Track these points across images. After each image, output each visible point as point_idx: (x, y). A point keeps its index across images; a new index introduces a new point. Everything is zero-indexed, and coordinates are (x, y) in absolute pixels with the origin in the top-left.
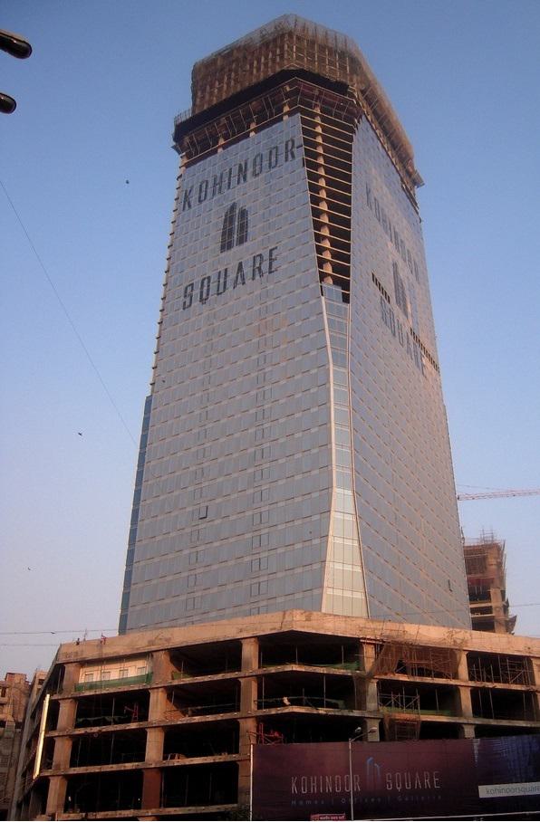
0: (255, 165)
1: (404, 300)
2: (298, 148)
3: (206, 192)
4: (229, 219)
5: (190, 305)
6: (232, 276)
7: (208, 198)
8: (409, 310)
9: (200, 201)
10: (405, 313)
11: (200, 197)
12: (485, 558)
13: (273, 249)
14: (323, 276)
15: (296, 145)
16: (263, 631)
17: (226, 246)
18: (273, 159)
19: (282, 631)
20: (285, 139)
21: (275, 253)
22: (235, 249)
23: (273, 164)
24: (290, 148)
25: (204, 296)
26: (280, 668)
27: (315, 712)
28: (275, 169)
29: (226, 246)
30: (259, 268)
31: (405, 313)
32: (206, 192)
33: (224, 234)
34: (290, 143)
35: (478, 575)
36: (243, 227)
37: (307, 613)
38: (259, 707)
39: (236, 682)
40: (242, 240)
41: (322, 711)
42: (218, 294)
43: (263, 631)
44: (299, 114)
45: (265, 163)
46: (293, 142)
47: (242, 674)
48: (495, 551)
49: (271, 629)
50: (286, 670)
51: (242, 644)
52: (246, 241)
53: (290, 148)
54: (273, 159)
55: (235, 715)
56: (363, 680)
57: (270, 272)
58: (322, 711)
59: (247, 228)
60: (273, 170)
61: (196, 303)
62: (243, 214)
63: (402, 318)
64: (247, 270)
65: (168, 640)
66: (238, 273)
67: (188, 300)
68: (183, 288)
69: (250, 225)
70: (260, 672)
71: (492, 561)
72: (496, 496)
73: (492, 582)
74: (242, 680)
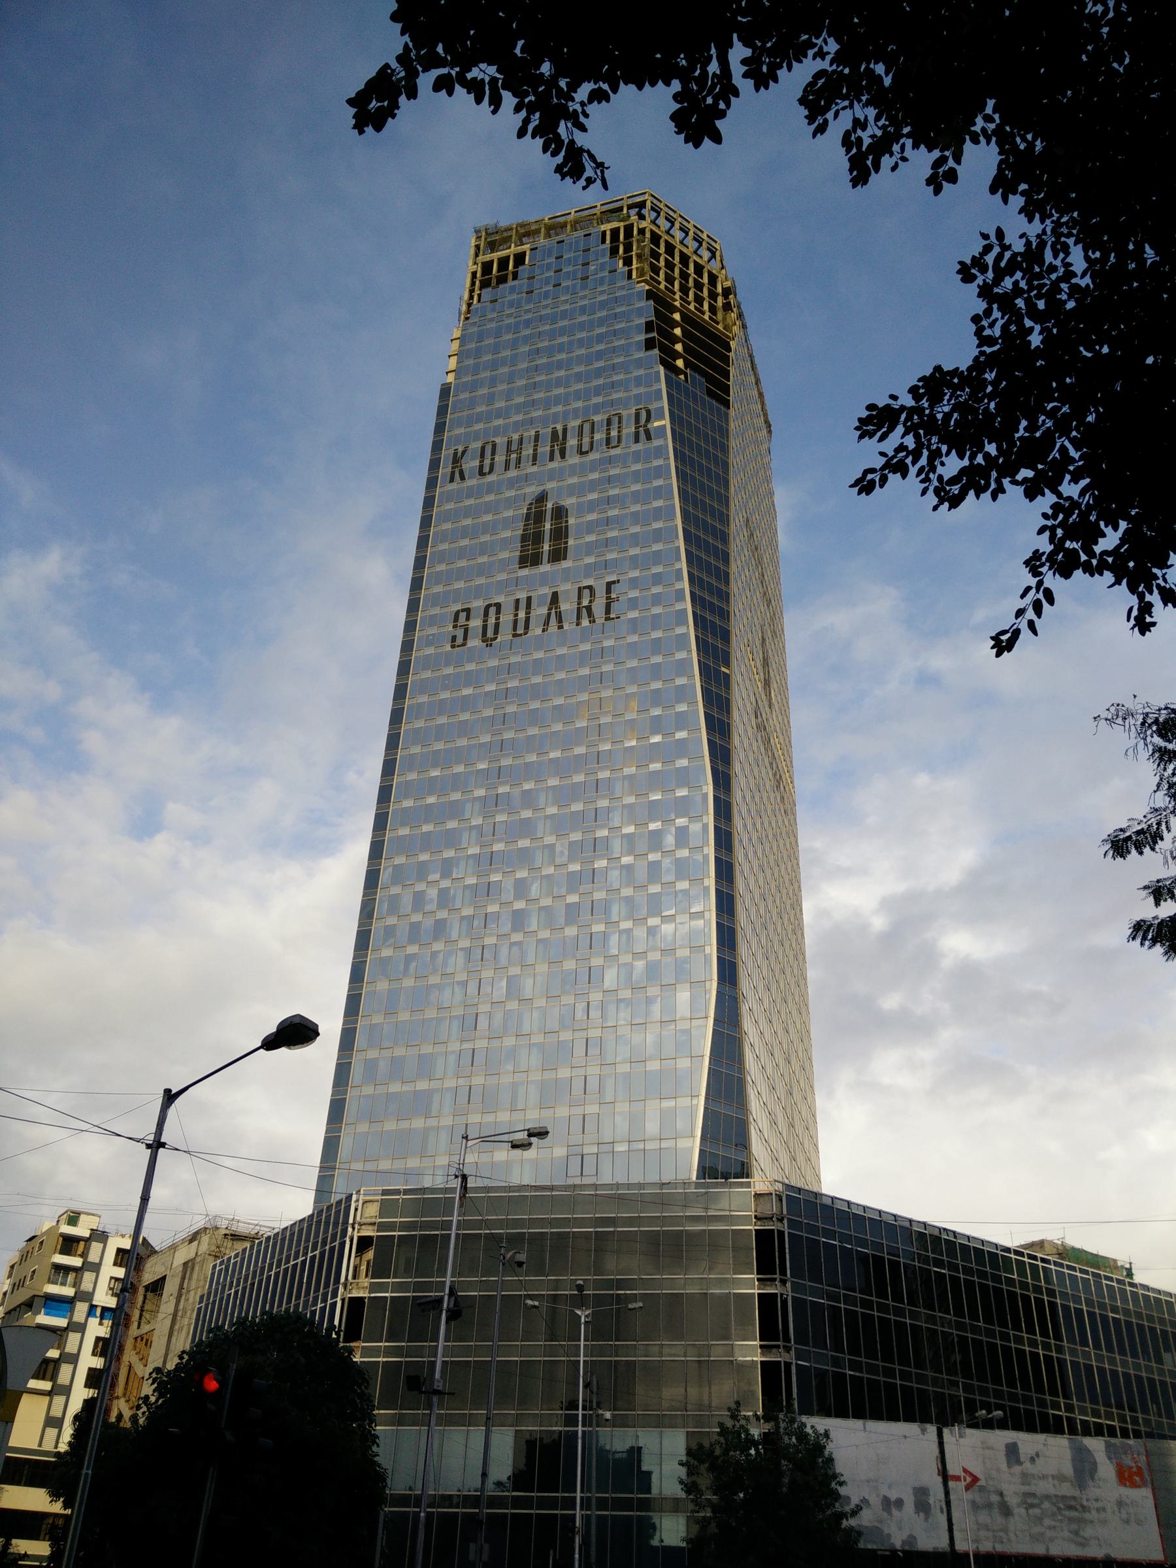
4: (535, 515)
17: (530, 559)
33: (524, 538)
36: (560, 534)
62: (560, 513)
66: (550, 609)
67: (460, 633)
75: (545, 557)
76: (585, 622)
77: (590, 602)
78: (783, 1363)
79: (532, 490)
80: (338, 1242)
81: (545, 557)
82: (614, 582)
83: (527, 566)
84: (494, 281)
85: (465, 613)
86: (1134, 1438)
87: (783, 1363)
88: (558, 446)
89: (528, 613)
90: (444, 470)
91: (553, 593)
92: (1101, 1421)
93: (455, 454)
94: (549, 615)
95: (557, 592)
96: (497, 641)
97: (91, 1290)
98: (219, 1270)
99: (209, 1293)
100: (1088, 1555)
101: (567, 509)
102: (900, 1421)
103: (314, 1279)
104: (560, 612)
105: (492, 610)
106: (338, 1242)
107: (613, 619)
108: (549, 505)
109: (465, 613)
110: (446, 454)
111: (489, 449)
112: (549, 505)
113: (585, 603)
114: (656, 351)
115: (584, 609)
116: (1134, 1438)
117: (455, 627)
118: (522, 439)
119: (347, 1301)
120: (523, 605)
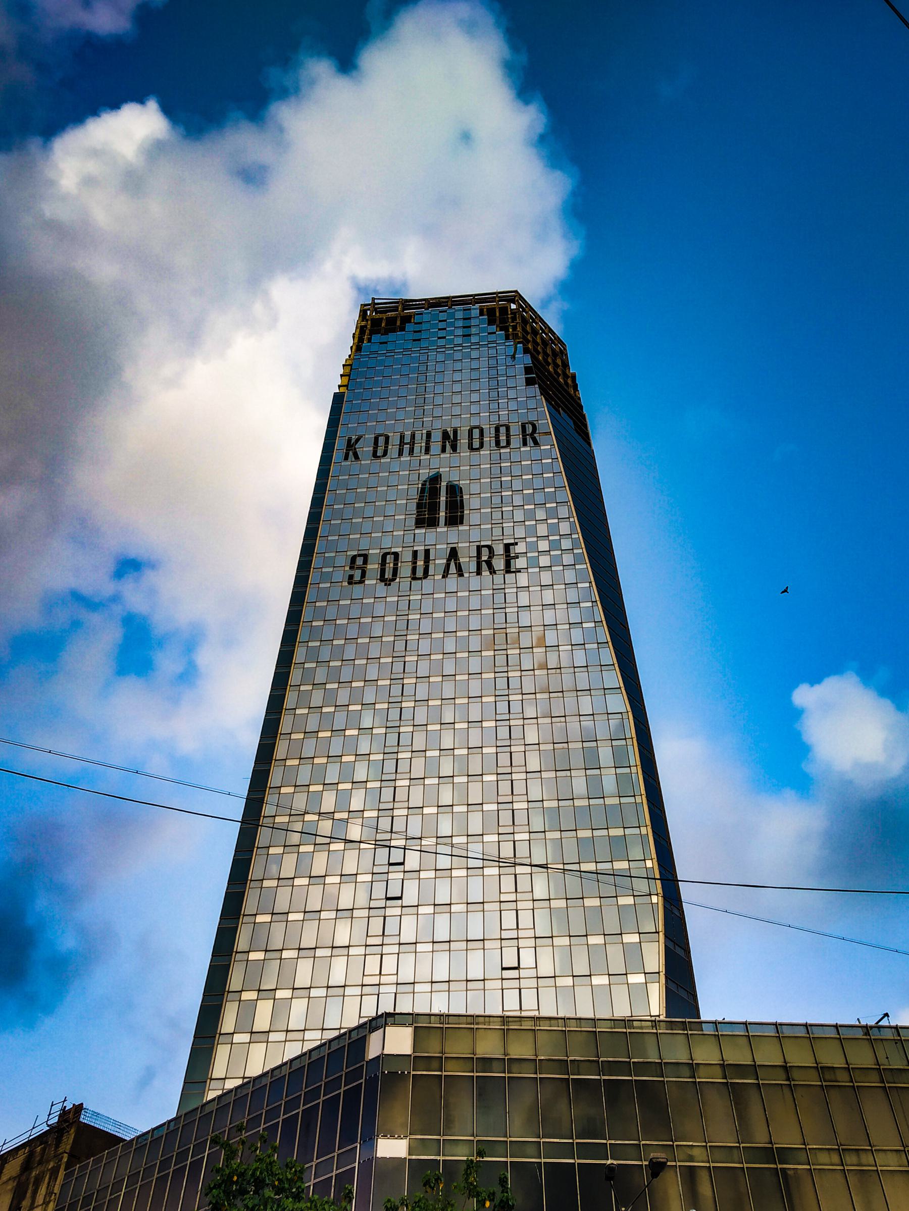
66: (449, 560)
75: (442, 521)
76: (485, 573)
77: (490, 557)
78: (526, 376)
79: (425, 473)
80: (155, 1177)
81: (442, 521)
82: (512, 544)
83: (424, 527)
84: (383, 331)
85: (362, 558)
86: (367, 565)
87: (526, 376)
88: (449, 442)
93: (350, 440)
95: (455, 548)
96: (396, 581)
100: (792, 1022)
101: (461, 488)
103: (300, 1120)
104: (459, 563)
105: (390, 559)
106: (155, 1177)
108: (444, 484)
109: (362, 558)
111: (381, 440)
112: (444, 484)
113: (484, 558)
115: (483, 563)
116: (367, 565)
117: (351, 568)
118: (414, 435)
120: (421, 556)
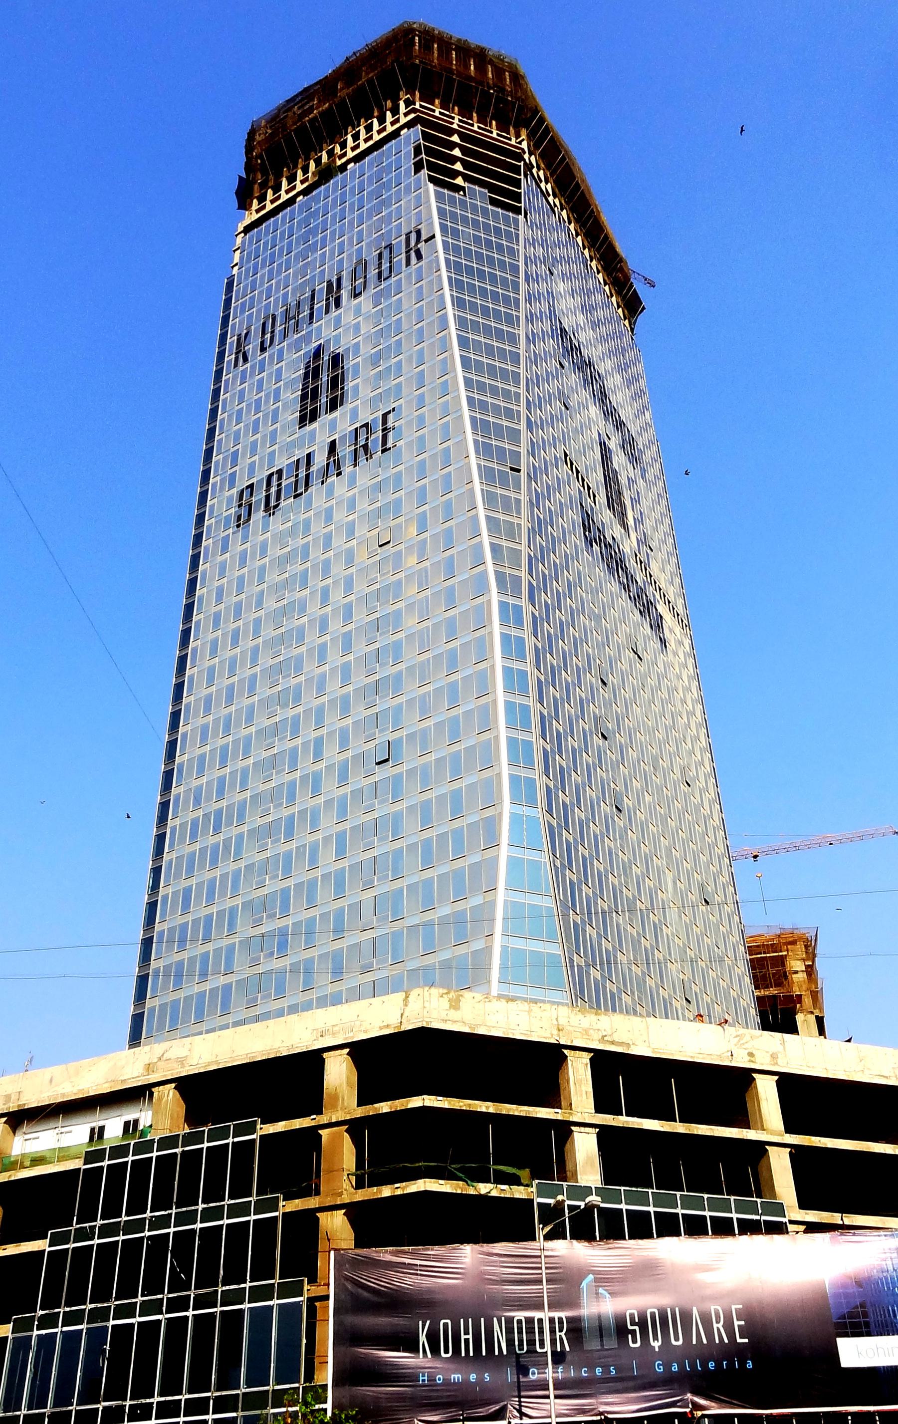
0: (354, 277)
1: (622, 504)
2: (426, 241)
3: (272, 332)
4: (312, 373)
5: (249, 520)
6: (320, 460)
7: (277, 341)
8: (631, 522)
9: (263, 349)
10: (625, 526)
11: (262, 343)
12: (782, 961)
13: (389, 412)
14: (418, 167)
15: (424, 237)
16: (365, 1031)
17: (308, 416)
18: (385, 266)
19: (403, 1028)
20: (404, 231)
21: (391, 417)
22: (324, 419)
23: (385, 274)
24: (413, 243)
25: (273, 503)
26: (400, 1104)
27: (472, 1191)
28: (388, 282)
29: (308, 416)
30: (365, 447)
31: (625, 526)
32: (272, 332)
33: (304, 397)
34: (413, 237)
35: (773, 991)
36: (336, 382)
37: (452, 995)
38: (359, 1185)
39: (312, 1136)
40: (334, 405)
41: (484, 1188)
42: (296, 497)
43: (365, 1031)
44: (419, 126)
45: (373, 272)
46: (418, 233)
47: (323, 1119)
48: (800, 947)
49: (381, 1028)
50: (411, 1105)
51: (323, 1060)
52: (342, 404)
53: (413, 243)
54: (385, 266)
55: (312, 1203)
56: (564, 1129)
57: (383, 451)
58: (484, 1188)
59: (343, 383)
60: (384, 285)
61: (259, 515)
62: (336, 360)
63: (617, 531)
64: (345, 451)
65: (181, 1061)
66: (328, 458)
67: (243, 511)
68: (235, 491)
69: (349, 376)
70: (360, 1112)
71: (796, 965)
72: (797, 848)
73: (800, 1002)
74: (324, 1133)
89: (308, 469)
90: (229, 358)
91: (331, 442)
92: (756, 1217)
94: (328, 465)
97: (586, 1057)
98: (234, 307)
99: (492, 188)
102: (678, 1234)
107: (390, 449)
110: (231, 340)
114: (425, 172)
119: (812, 1216)
